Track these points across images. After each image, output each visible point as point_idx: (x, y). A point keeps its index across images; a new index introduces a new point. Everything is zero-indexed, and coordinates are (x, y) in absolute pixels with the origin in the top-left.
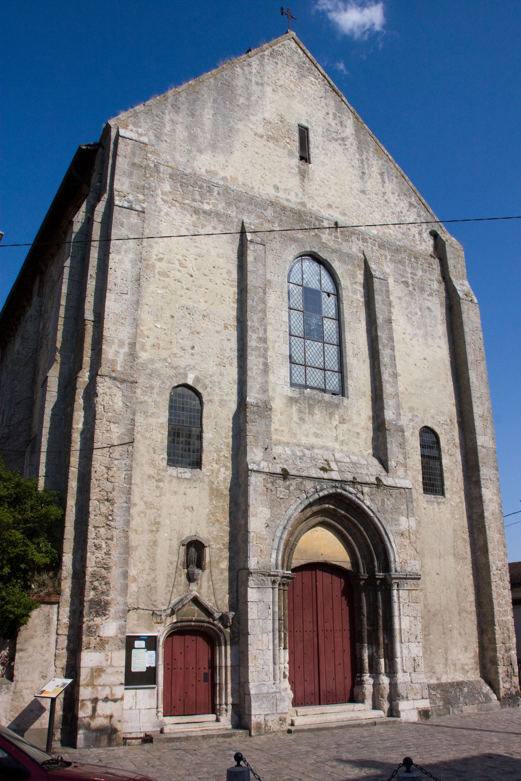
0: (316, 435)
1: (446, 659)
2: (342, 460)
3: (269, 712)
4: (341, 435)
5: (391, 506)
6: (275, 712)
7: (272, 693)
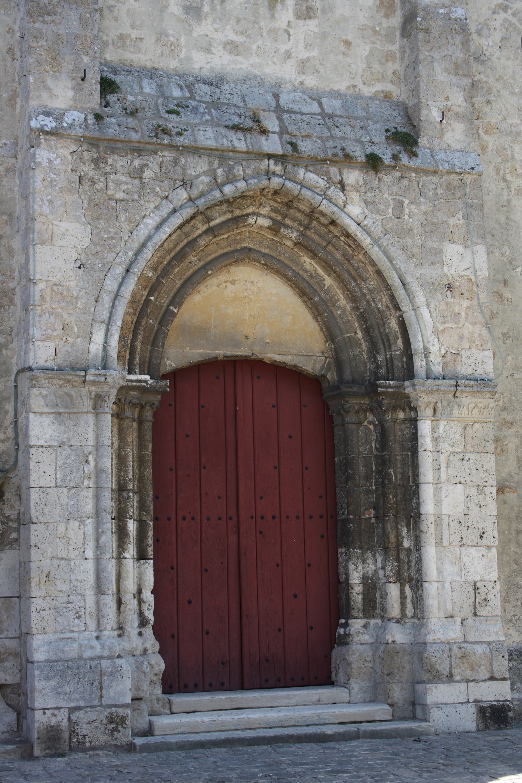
0: (232, 48)
2: (296, 108)
3: (81, 704)
4: (301, 45)
5: (422, 218)
6: (96, 702)
7: (92, 659)
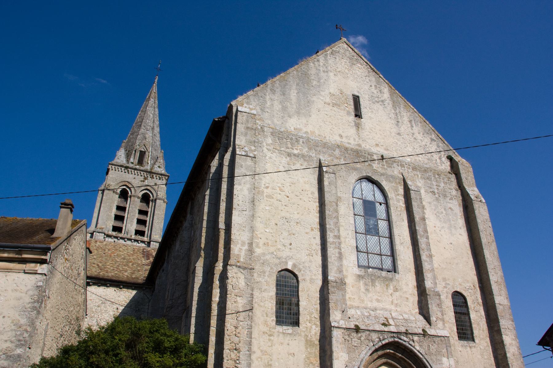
0: (378, 301)
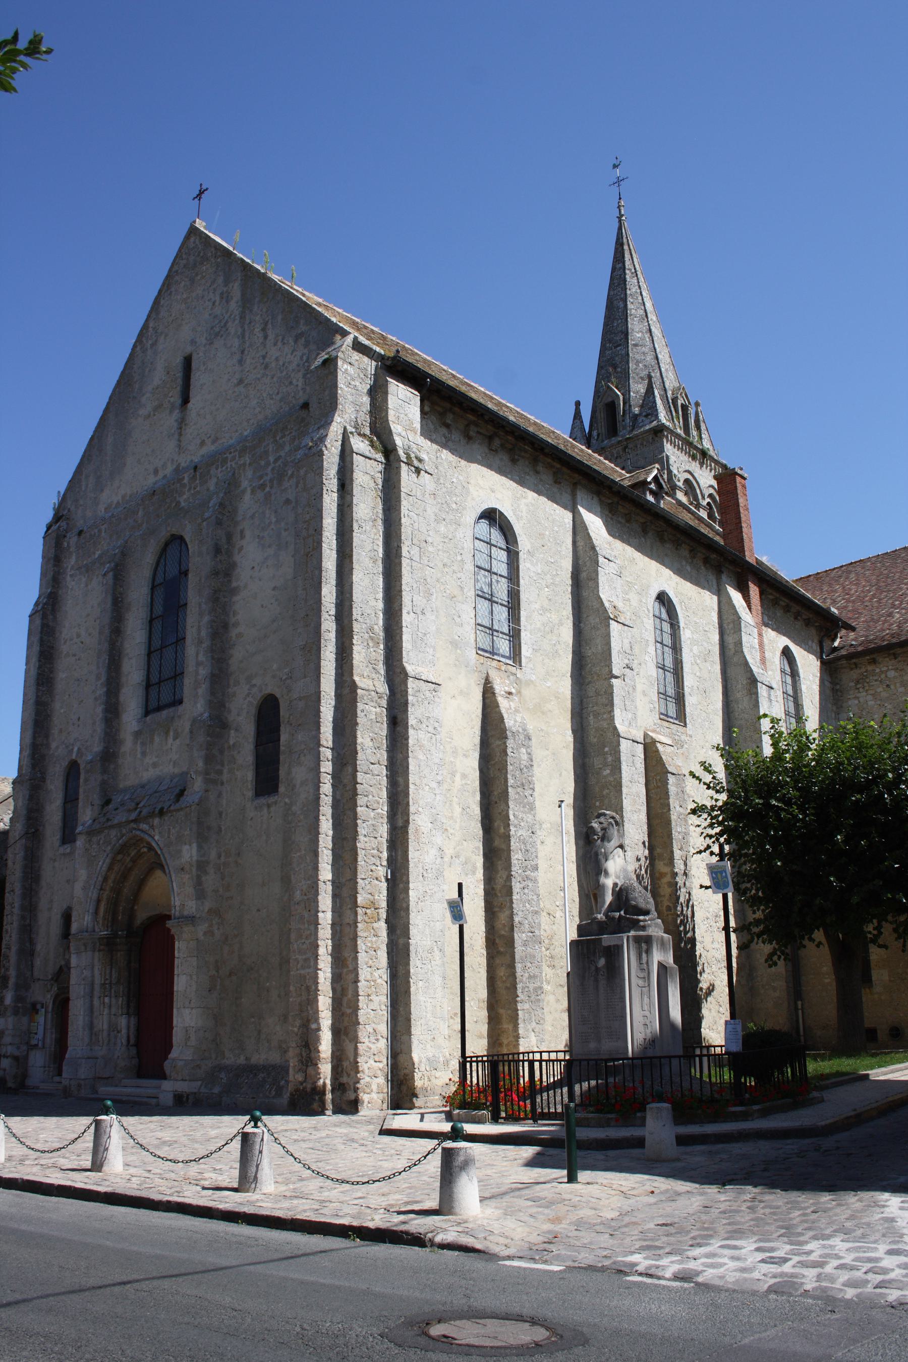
1: (259, 1032)
